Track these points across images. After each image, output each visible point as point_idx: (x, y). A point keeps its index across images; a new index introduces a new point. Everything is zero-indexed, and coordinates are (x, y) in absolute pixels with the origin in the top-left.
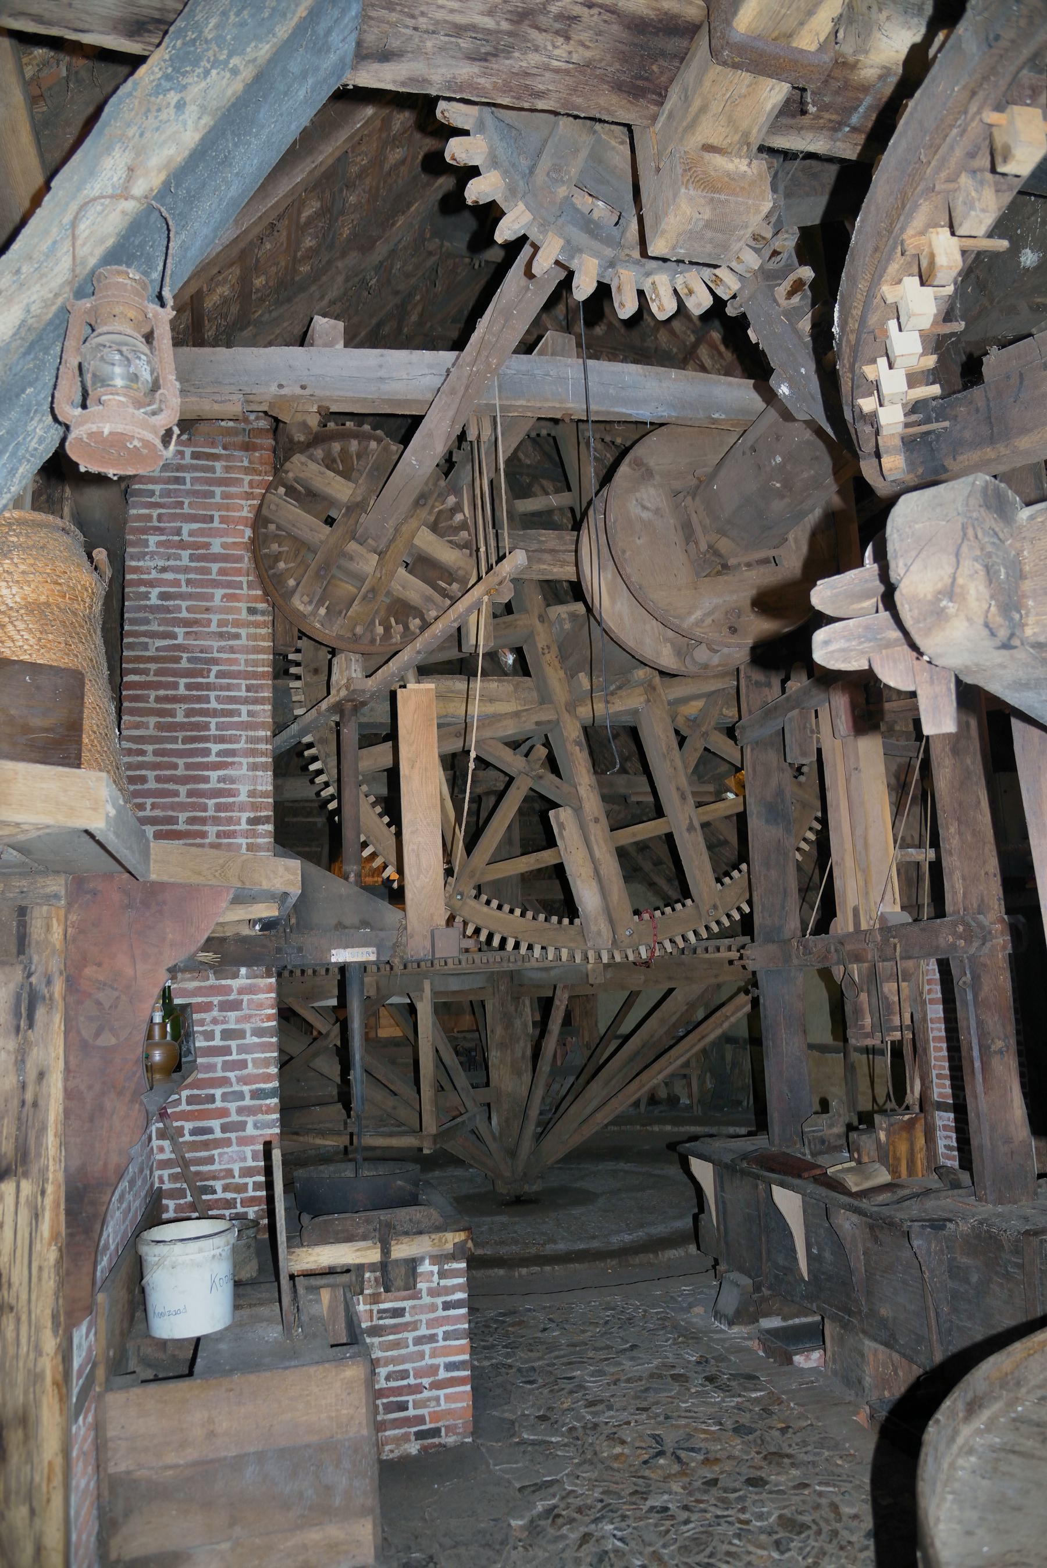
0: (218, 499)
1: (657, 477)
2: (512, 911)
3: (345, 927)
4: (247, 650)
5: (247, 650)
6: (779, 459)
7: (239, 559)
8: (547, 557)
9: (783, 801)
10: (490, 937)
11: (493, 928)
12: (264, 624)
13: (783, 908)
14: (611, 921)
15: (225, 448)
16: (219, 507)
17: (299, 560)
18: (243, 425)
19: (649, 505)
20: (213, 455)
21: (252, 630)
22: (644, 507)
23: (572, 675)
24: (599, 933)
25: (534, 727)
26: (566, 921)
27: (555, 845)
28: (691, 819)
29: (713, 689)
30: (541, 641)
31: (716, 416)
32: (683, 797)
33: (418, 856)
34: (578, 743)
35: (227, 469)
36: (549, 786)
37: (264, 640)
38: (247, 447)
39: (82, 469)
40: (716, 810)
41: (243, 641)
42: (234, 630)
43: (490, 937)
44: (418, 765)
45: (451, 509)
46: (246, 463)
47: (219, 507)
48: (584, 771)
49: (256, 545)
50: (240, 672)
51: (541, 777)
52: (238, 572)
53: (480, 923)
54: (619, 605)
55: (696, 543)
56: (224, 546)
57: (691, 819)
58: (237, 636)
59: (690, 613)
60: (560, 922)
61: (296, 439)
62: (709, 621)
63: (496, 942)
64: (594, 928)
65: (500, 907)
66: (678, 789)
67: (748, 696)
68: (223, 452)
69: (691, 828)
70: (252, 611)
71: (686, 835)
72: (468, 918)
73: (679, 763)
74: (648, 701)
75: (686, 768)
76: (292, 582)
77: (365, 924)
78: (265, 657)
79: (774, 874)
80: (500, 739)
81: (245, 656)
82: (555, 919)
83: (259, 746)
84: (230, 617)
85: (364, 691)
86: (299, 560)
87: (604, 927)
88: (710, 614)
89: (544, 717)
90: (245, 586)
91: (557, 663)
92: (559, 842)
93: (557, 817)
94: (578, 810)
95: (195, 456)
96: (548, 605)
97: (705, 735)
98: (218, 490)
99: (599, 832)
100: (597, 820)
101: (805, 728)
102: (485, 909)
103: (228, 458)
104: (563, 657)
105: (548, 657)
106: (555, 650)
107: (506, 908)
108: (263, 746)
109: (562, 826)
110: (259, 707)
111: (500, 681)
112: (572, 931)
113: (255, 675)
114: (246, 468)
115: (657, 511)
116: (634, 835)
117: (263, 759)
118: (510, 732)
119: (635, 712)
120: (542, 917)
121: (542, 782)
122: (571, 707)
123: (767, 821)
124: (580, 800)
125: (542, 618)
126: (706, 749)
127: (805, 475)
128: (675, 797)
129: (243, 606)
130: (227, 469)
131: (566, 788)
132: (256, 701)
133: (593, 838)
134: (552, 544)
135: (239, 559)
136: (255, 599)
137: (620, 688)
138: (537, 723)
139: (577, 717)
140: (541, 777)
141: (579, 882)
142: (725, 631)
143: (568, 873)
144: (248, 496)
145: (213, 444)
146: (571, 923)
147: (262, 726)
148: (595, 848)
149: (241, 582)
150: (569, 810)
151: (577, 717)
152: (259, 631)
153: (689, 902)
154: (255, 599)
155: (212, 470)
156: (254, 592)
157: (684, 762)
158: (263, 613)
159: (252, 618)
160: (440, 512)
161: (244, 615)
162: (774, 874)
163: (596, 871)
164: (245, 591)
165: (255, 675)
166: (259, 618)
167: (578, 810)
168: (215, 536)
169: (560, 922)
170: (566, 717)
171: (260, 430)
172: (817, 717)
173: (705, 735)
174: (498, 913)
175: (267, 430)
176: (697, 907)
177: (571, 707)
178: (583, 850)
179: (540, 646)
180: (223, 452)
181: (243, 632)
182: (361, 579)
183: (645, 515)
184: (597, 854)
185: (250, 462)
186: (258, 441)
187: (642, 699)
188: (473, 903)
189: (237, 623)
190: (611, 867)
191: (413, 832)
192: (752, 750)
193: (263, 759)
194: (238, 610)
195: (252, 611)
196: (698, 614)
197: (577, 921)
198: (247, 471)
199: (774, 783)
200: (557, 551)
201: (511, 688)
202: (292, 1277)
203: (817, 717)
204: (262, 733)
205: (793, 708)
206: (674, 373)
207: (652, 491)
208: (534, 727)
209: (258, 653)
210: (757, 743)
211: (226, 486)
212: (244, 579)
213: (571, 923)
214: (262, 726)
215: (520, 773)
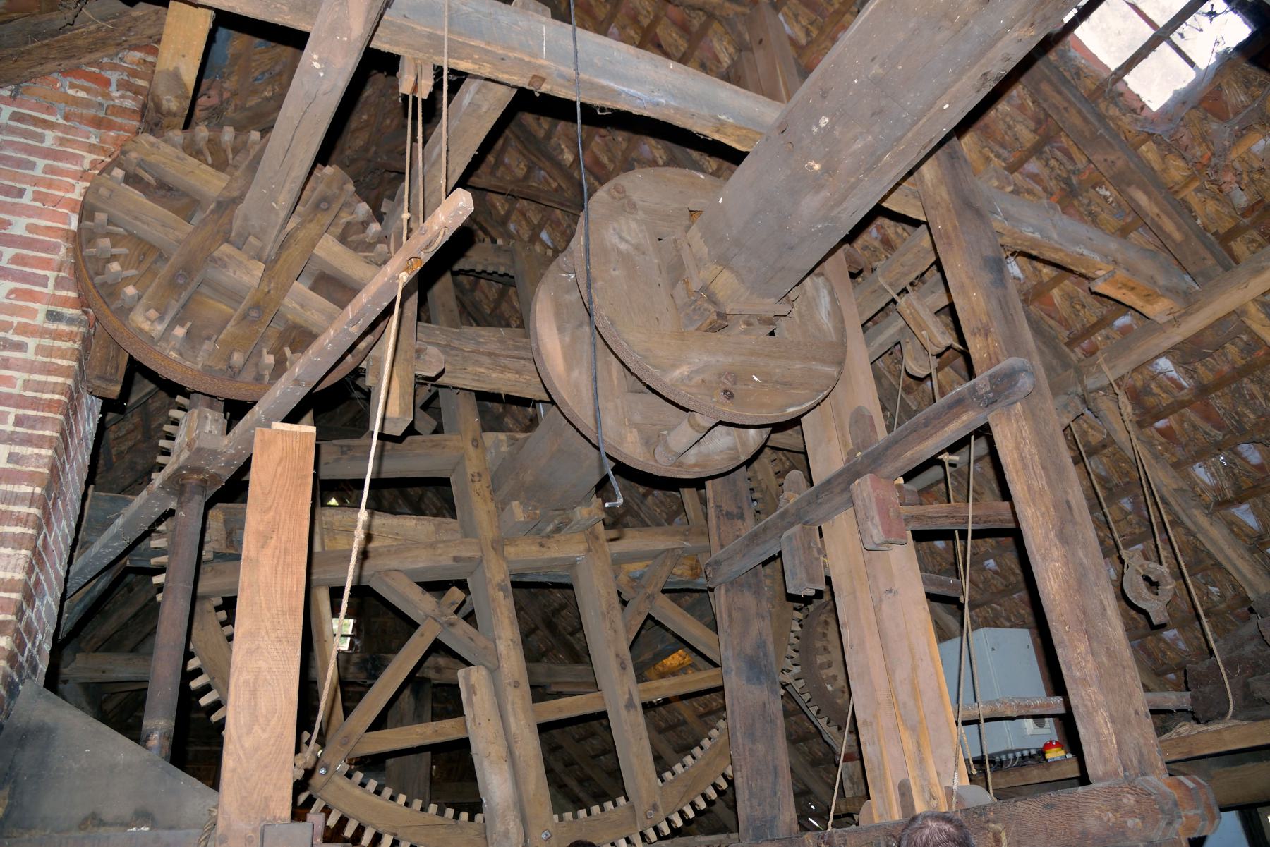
0: (38, 172)
1: (640, 213)
2: (393, 798)
3: (102, 823)
4: (31, 367)
5: (31, 367)
6: (824, 121)
7: (52, 248)
8: (486, 360)
9: (765, 655)
10: (343, 821)
11: (365, 819)
12: (70, 337)
13: (775, 794)
14: (524, 820)
15: (66, 118)
16: (36, 182)
17: (144, 266)
18: (100, 99)
19: (628, 238)
20: (45, 121)
21: (47, 342)
22: (622, 239)
23: (502, 506)
24: (506, 834)
25: (451, 563)
26: (464, 816)
27: (461, 714)
28: (630, 694)
29: (661, 546)
30: (472, 467)
31: (723, 117)
32: (623, 667)
33: (254, 692)
34: (502, 588)
35: (62, 141)
36: (459, 637)
37: (63, 357)
38: (98, 123)
39: (154, 475)
40: (657, 689)
41: (30, 354)
42: (16, 338)
43: (343, 821)
44: (273, 542)
45: (362, 223)
46: (93, 140)
47: (36, 182)
48: (506, 622)
49: (80, 240)
50: (10, 396)
51: (452, 625)
52: (46, 264)
53: (348, 811)
54: (575, 374)
55: (686, 282)
56: (30, 228)
57: (630, 694)
58: (20, 347)
59: (674, 367)
60: (456, 817)
61: (165, 105)
62: (697, 379)
63: (349, 832)
64: (500, 827)
65: (378, 792)
66: (617, 656)
67: (719, 528)
68: (61, 121)
69: (630, 705)
70: (52, 316)
71: (624, 712)
72: (332, 802)
73: (620, 625)
74: (589, 550)
75: (627, 632)
76: (130, 290)
77: (143, 816)
78: (60, 380)
79: (761, 748)
80: (409, 574)
81: (26, 376)
82: (450, 812)
83: (16, 509)
84: (15, 320)
85: (215, 453)
86: (144, 266)
87: (514, 827)
88: (697, 372)
89: (465, 553)
90: (51, 283)
91: (487, 494)
92: (466, 710)
93: (467, 678)
94: (494, 671)
95: (15, 117)
96: (484, 430)
97: (651, 597)
98: (41, 163)
99: (518, 699)
100: (516, 685)
101: (810, 547)
102: (358, 791)
103: (66, 129)
104: (494, 488)
105: (477, 485)
106: (486, 480)
107: (387, 792)
108: (23, 509)
109: (472, 690)
110: (30, 451)
111: (418, 520)
112: (472, 830)
113: (35, 404)
114: (90, 145)
115: (637, 247)
116: (560, 710)
117: (19, 530)
118: (420, 565)
119: (573, 565)
120: (433, 808)
121: (452, 630)
122: (499, 545)
123: (749, 680)
124: (497, 656)
125: (476, 443)
126: (649, 617)
127: (858, 145)
128: (614, 664)
129: (41, 308)
130: (62, 141)
131: (481, 641)
132: (28, 441)
133: (509, 707)
134: (492, 347)
135: (52, 248)
136: (65, 302)
137: (558, 530)
138: (456, 559)
139: (504, 558)
140: (452, 625)
141: (486, 764)
142: (719, 396)
143: (474, 751)
144: (82, 176)
145: (49, 110)
146: (471, 819)
147: (31, 478)
148: (512, 720)
149: (47, 278)
150: (483, 671)
151: (504, 558)
152: (58, 343)
153: (621, 800)
154: (65, 302)
155: (41, 138)
156: (64, 293)
157: (626, 626)
158: (71, 321)
159: (51, 326)
160: (348, 224)
161: (40, 320)
162: (761, 748)
163: (510, 752)
164: (50, 289)
165: (35, 404)
166: (63, 327)
167: (494, 671)
168: (19, 215)
169: (456, 817)
170: (491, 555)
171: (123, 111)
172: (821, 535)
173: (651, 597)
174: (375, 798)
175: (134, 111)
176: (633, 807)
177: (499, 545)
178: (496, 721)
179: (470, 471)
180: (61, 121)
181: (32, 343)
182: (233, 296)
183: (623, 246)
184: (513, 727)
185: (102, 141)
186: (119, 120)
187: (583, 547)
188: (343, 782)
189: (23, 329)
190: (530, 747)
191: (250, 652)
192: (727, 591)
193: (19, 530)
194: (33, 313)
195: (52, 316)
196: (684, 370)
197: (479, 817)
198: (91, 148)
199: (754, 632)
200: (498, 356)
201: (432, 528)
202: (984, 432)
203: (821, 535)
204: (26, 489)
205: (792, 524)
206: (672, 64)
207: (634, 225)
208: (451, 563)
209: (50, 373)
210: (731, 583)
211: (55, 159)
212: (52, 275)
213: (471, 819)
214: (31, 478)
215: (427, 616)
